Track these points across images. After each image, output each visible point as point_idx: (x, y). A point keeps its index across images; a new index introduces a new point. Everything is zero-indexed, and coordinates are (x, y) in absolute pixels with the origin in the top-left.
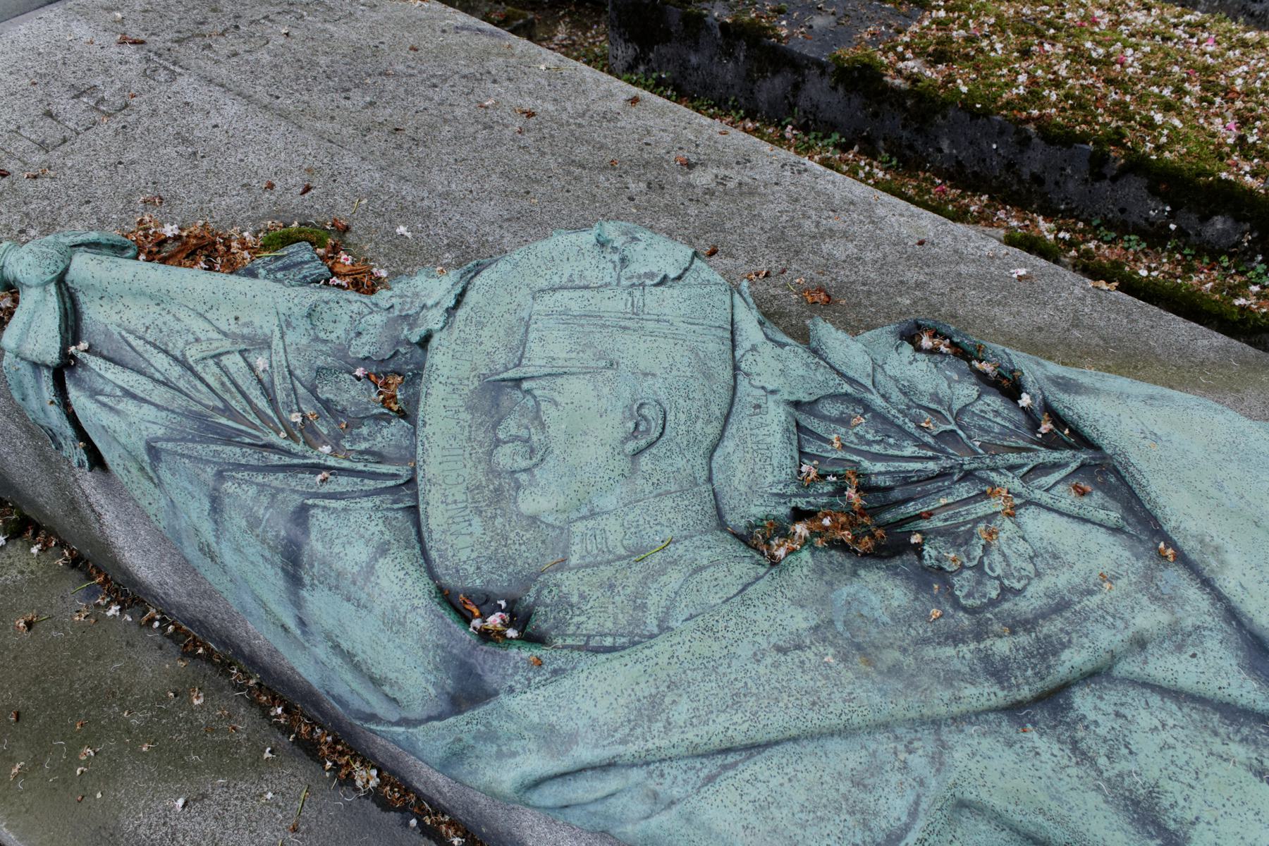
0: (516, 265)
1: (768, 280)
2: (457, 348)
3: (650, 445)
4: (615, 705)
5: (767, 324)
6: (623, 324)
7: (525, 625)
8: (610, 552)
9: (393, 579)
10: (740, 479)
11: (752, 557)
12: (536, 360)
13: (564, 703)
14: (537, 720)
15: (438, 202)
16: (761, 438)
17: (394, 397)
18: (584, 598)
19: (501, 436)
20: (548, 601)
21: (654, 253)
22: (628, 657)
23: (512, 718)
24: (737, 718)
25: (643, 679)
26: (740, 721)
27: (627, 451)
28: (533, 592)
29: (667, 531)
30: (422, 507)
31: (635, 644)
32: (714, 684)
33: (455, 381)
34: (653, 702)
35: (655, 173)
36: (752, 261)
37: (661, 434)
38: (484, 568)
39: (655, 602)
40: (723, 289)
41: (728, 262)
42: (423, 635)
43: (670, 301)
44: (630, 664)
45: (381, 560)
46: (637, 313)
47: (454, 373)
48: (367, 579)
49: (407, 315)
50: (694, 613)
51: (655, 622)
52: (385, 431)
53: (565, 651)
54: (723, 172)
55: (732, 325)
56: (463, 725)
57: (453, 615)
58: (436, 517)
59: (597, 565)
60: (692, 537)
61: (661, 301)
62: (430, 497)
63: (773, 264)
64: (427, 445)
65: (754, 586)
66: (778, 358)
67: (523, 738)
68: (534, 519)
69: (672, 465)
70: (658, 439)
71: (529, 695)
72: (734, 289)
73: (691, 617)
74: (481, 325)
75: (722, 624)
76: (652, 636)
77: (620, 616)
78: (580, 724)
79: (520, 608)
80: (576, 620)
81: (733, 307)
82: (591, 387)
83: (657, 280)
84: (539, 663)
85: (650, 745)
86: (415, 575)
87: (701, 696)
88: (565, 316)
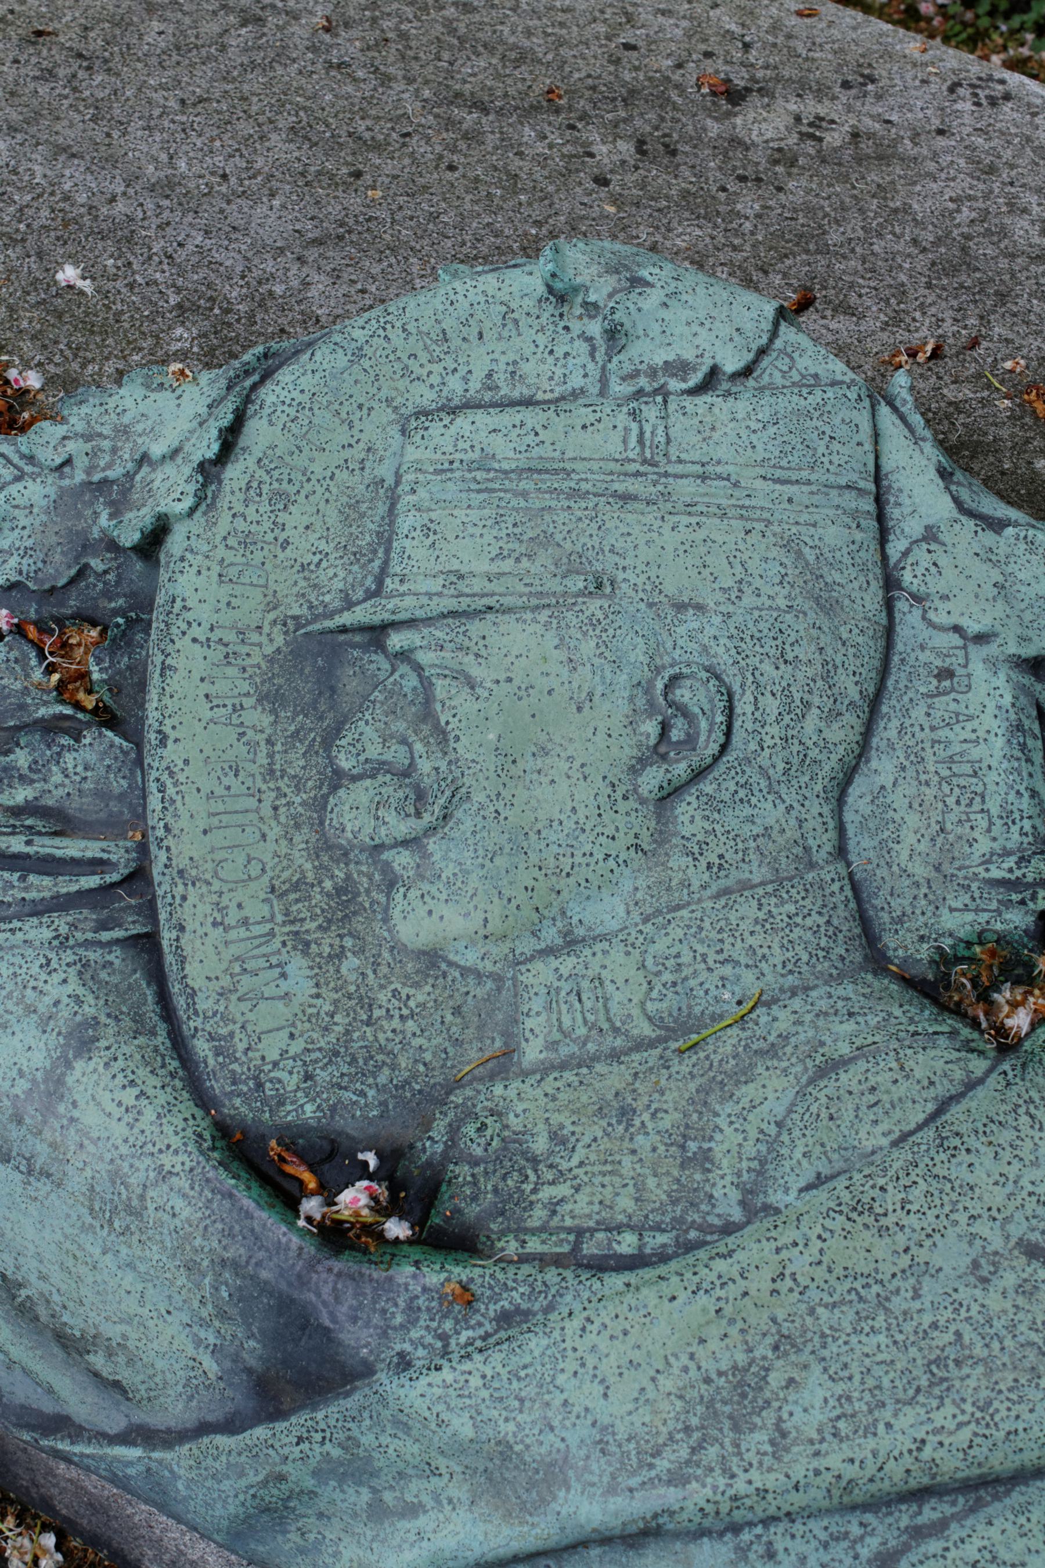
0: (359, 354)
1: (938, 367)
2: (229, 556)
3: (698, 774)
4: (651, 1394)
5: (959, 476)
6: (619, 487)
7: (427, 1208)
8: (616, 1030)
9: (111, 1107)
10: (912, 847)
11: (953, 1034)
12: (419, 578)
13: (531, 1391)
14: (467, 1431)
15: (149, 205)
16: (957, 748)
17: (83, 676)
18: (563, 1142)
19: (345, 763)
20: (479, 1151)
21: (686, 314)
22: (675, 1276)
23: (407, 1428)
24: (944, 1417)
25: (714, 1332)
26: (951, 1425)
27: (644, 791)
28: (439, 1129)
29: (749, 977)
30: (167, 937)
31: (690, 1247)
32: (882, 1339)
33: (230, 637)
34: (741, 1384)
35: (651, 116)
36: (896, 320)
37: (724, 748)
38: (322, 1076)
39: (731, 1146)
40: (852, 395)
41: (842, 324)
42: (189, 1238)
43: (725, 431)
44: (683, 1296)
45: (79, 1065)
46: (652, 460)
47: (226, 617)
48: (48, 1110)
49: (105, 481)
50: (826, 1171)
51: (735, 1195)
52: (69, 758)
53: (526, 1269)
54: (811, 108)
55: (877, 479)
56: (283, 1443)
57: (256, 1190)
58: (201, 958)
59: (588, 1062)
60: (807, 989)
61: (707, 431)
62: (186, 913)
63: (948, 327)
64: (171, 791)
65: (965, 1104)
66: (988, 556)
67: (436, 1473)
68: (431, 959)
69: (751, 820)
70: (716, 759)
71: (447, 1375)
72: (878, 394)
73: (819, 1181)
74: (283, 500)
75: (893, 1197)
76: (729, 1229)
77: (651, 1182)
78: (573, 1440)
79: (411, 1169)
80: (546, 1193)
81: (876, 436)
82: (551, 639)
83: (695, 379)
84: (467, 1297)
85: (740, 1486)
86: (163, 1098)
87: (855, 1369)
88: (481, 472)
